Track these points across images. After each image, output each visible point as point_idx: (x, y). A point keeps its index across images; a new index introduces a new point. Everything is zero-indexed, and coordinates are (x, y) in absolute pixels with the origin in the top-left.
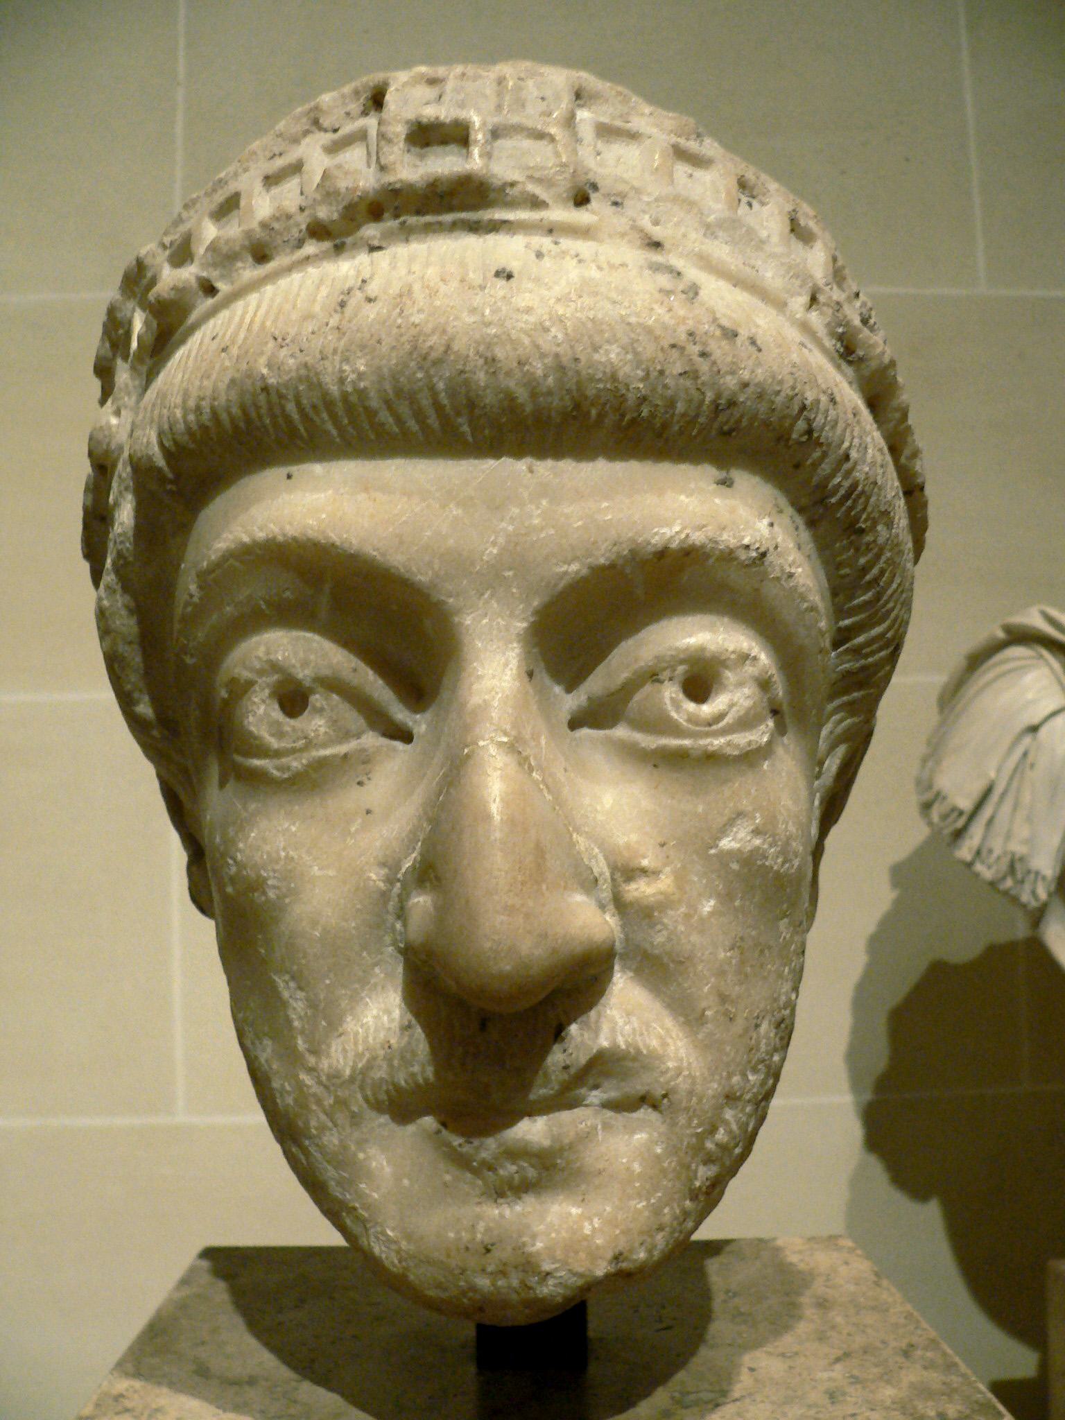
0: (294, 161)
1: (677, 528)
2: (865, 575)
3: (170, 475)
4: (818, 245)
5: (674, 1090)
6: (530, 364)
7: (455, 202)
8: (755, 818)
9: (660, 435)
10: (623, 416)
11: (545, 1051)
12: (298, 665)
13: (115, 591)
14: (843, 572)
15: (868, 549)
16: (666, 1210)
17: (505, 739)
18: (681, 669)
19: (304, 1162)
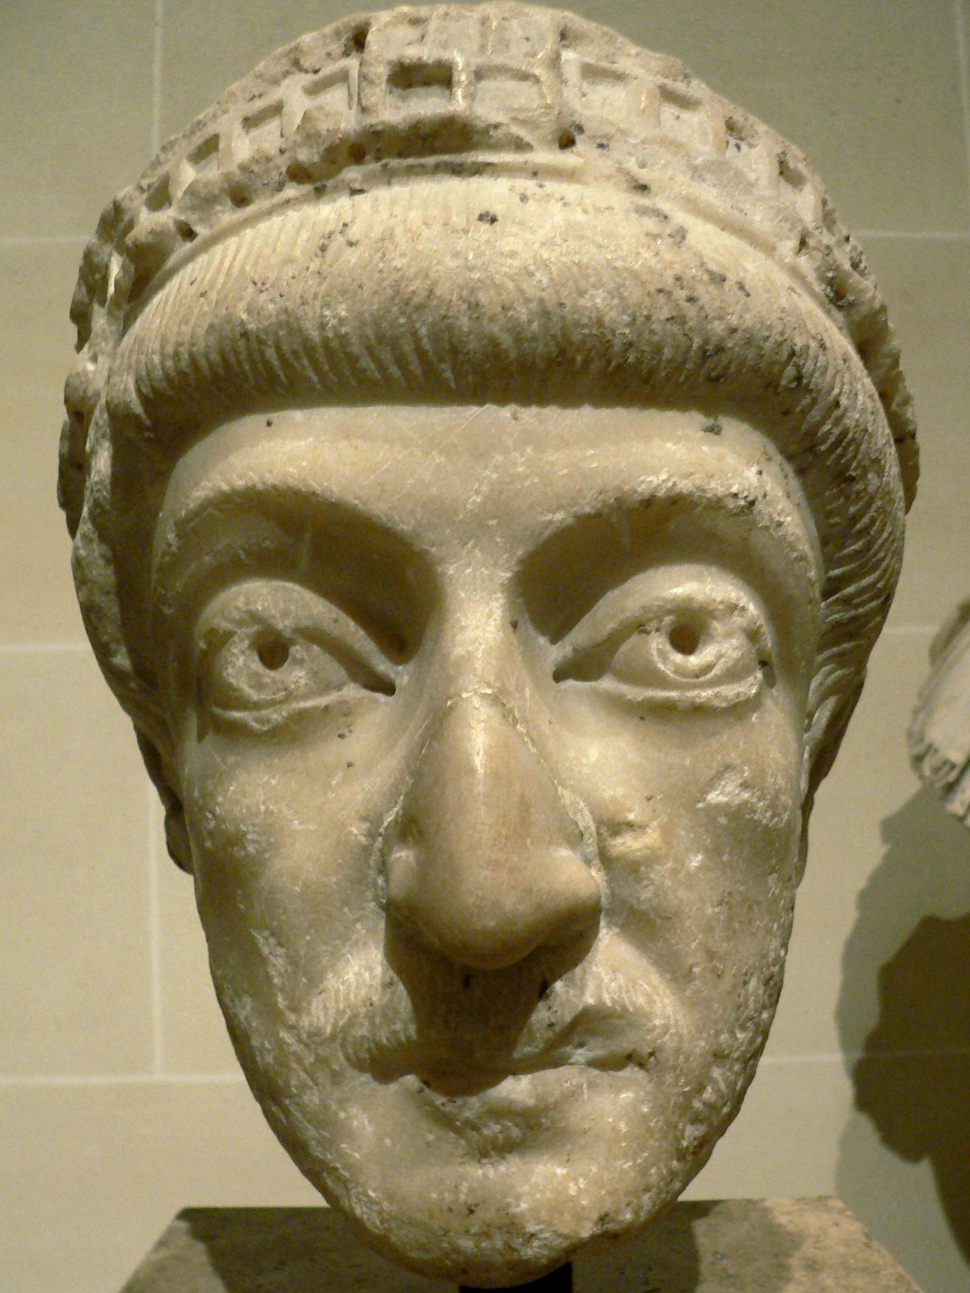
1: (664, 477)
2: (855, 524)
4: (808, 188)
6: (515, 309)
7: (438, 144)
8: (743, 771)
10: (609, 362)
11: (529, 1008)
12: (278, 616)
13: (91, 540)
16: (653, 1171)
17: (489, 691)
18: (668, 619)
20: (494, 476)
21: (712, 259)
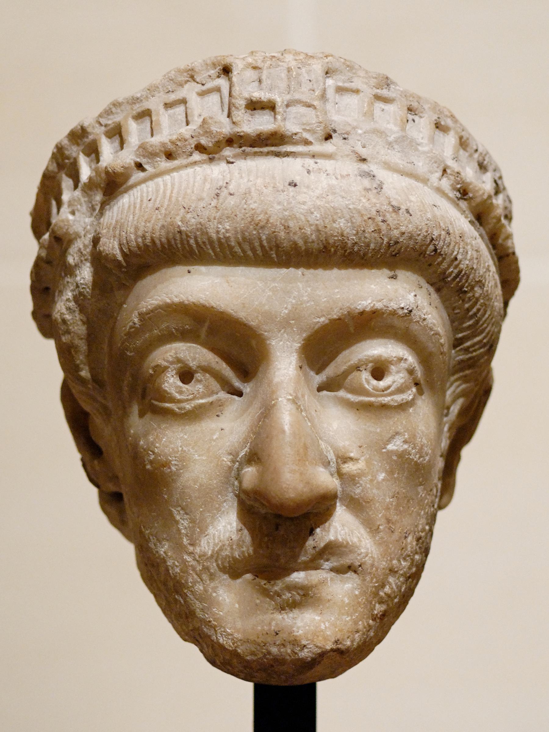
0: (181, 98)
1: (370, 302)
2: (469, 312)
3: (124, 264)
4: (452, 133)
5: (365, 563)
6: (305, 229)
7: (269, 142)
8: (405, 435)
9: (363, 258)
10: (346, 251)
11: (305, 540)
12: (190, 360)
13: (74, 311)
16: (360, 623)
17: (291, 397)
18: (370, 365)
20: (294, 301)
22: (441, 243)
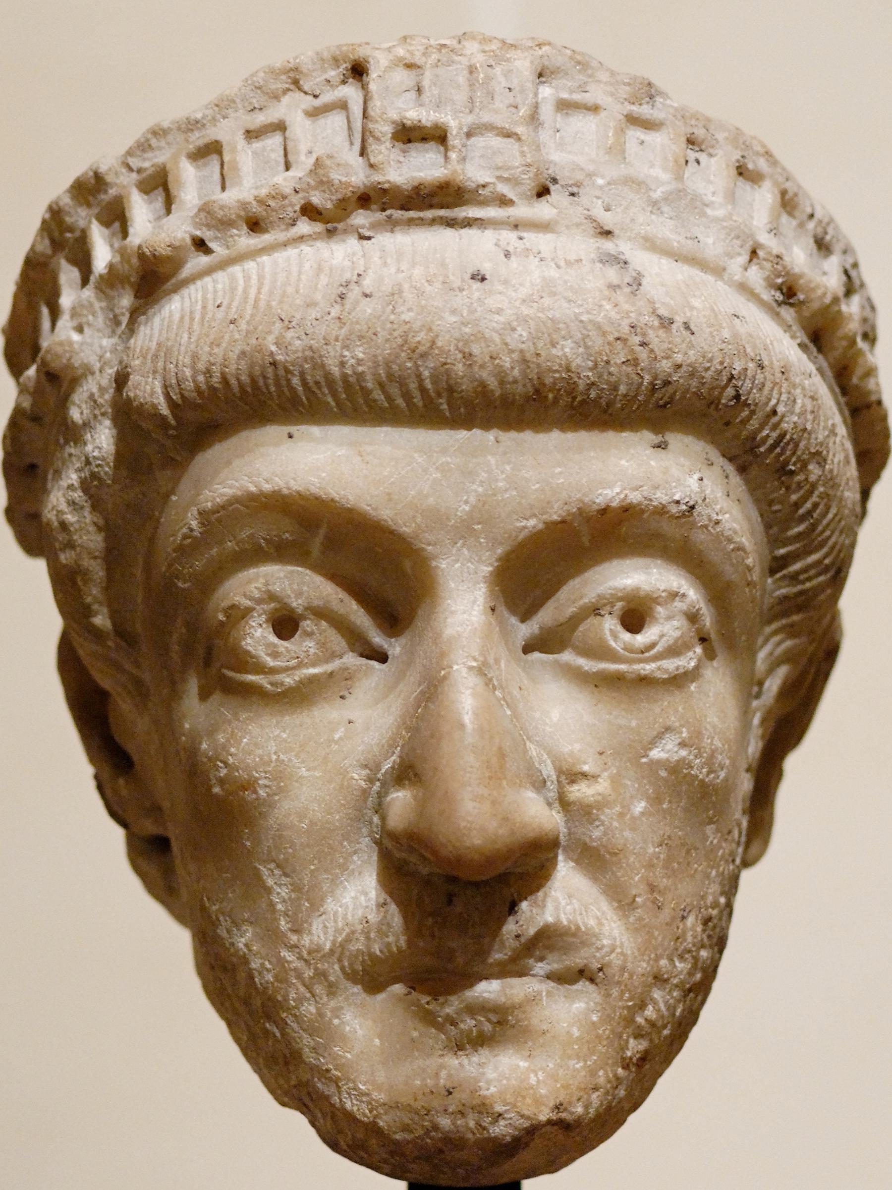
0: (276, 121)
1: (618, 490)
2: (797, 512)
3: (173, 422)
4: (767, 184)
5: (609, 964)
7: (435, 200)
8: (682, 733)
9: (605, 411)
10: (574, 398)
11: (501, 922)
12: (293, 596)
13: (82, 508)
14: (776, 507)
15: (799, 486)
16: (601, 1073)
17: (474, 664)
18: (619, 605)
19: (278, 1034)
20: (480, 489)
21: (663, 303)
22: (748, 384)
